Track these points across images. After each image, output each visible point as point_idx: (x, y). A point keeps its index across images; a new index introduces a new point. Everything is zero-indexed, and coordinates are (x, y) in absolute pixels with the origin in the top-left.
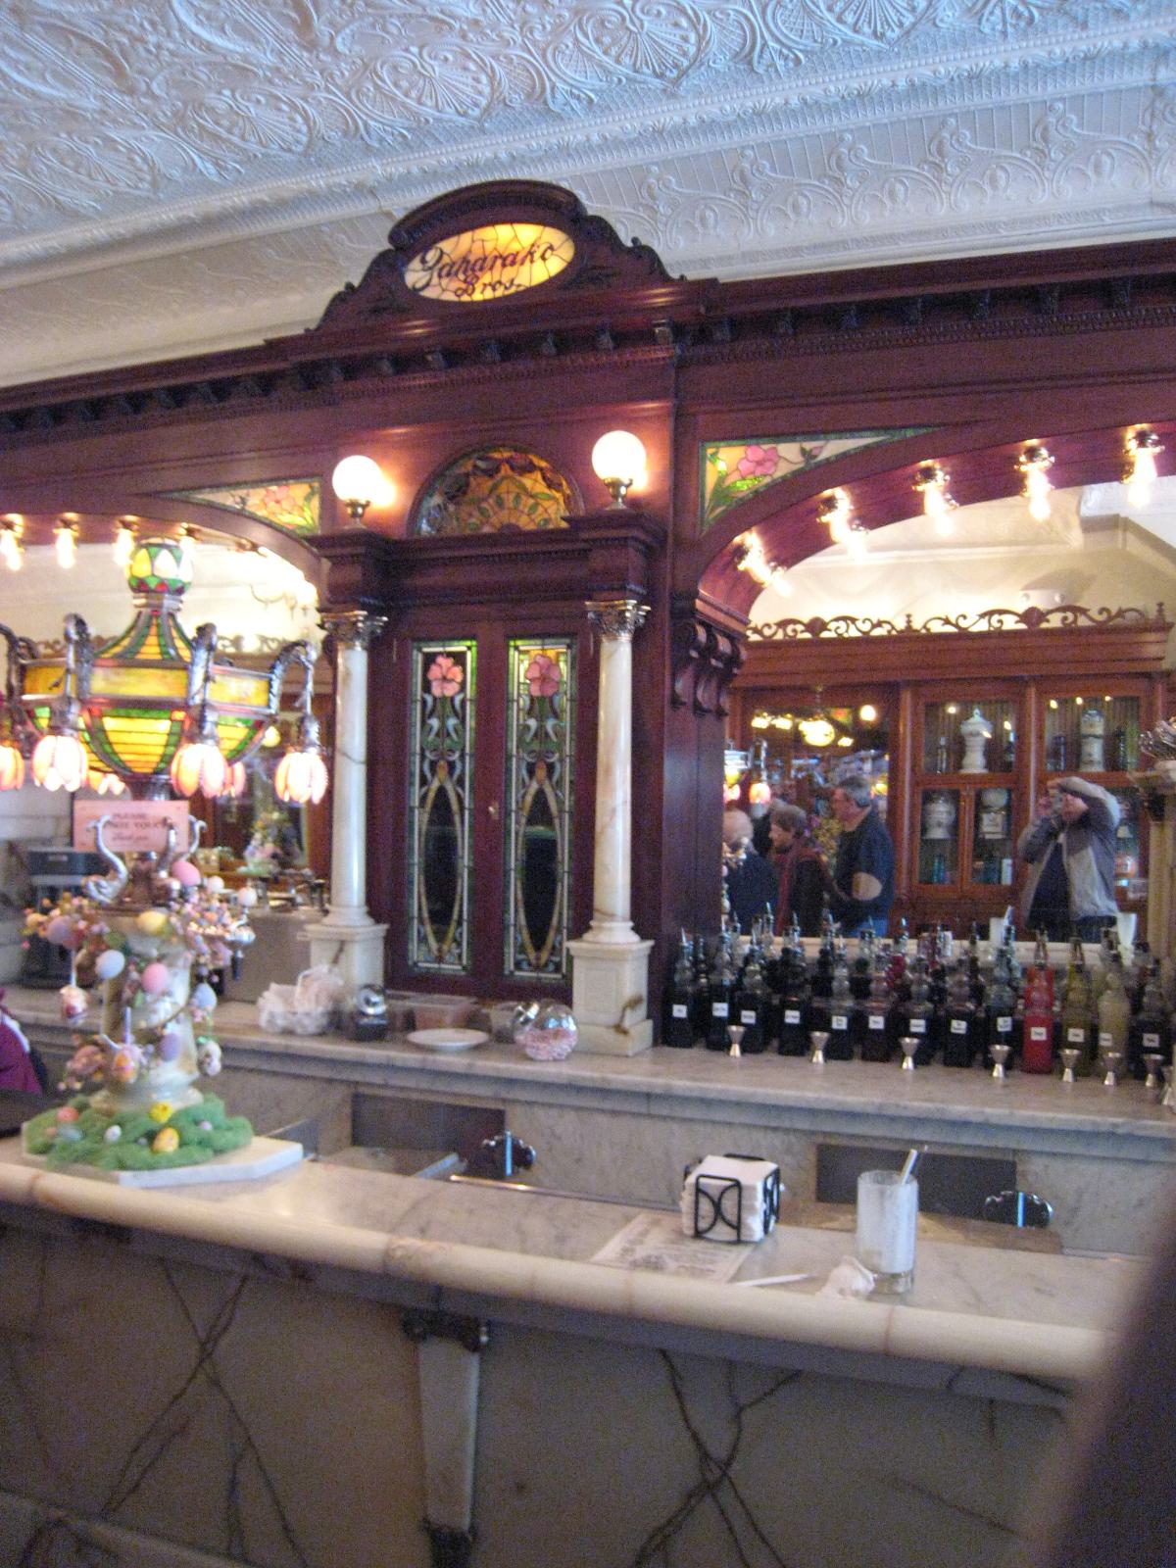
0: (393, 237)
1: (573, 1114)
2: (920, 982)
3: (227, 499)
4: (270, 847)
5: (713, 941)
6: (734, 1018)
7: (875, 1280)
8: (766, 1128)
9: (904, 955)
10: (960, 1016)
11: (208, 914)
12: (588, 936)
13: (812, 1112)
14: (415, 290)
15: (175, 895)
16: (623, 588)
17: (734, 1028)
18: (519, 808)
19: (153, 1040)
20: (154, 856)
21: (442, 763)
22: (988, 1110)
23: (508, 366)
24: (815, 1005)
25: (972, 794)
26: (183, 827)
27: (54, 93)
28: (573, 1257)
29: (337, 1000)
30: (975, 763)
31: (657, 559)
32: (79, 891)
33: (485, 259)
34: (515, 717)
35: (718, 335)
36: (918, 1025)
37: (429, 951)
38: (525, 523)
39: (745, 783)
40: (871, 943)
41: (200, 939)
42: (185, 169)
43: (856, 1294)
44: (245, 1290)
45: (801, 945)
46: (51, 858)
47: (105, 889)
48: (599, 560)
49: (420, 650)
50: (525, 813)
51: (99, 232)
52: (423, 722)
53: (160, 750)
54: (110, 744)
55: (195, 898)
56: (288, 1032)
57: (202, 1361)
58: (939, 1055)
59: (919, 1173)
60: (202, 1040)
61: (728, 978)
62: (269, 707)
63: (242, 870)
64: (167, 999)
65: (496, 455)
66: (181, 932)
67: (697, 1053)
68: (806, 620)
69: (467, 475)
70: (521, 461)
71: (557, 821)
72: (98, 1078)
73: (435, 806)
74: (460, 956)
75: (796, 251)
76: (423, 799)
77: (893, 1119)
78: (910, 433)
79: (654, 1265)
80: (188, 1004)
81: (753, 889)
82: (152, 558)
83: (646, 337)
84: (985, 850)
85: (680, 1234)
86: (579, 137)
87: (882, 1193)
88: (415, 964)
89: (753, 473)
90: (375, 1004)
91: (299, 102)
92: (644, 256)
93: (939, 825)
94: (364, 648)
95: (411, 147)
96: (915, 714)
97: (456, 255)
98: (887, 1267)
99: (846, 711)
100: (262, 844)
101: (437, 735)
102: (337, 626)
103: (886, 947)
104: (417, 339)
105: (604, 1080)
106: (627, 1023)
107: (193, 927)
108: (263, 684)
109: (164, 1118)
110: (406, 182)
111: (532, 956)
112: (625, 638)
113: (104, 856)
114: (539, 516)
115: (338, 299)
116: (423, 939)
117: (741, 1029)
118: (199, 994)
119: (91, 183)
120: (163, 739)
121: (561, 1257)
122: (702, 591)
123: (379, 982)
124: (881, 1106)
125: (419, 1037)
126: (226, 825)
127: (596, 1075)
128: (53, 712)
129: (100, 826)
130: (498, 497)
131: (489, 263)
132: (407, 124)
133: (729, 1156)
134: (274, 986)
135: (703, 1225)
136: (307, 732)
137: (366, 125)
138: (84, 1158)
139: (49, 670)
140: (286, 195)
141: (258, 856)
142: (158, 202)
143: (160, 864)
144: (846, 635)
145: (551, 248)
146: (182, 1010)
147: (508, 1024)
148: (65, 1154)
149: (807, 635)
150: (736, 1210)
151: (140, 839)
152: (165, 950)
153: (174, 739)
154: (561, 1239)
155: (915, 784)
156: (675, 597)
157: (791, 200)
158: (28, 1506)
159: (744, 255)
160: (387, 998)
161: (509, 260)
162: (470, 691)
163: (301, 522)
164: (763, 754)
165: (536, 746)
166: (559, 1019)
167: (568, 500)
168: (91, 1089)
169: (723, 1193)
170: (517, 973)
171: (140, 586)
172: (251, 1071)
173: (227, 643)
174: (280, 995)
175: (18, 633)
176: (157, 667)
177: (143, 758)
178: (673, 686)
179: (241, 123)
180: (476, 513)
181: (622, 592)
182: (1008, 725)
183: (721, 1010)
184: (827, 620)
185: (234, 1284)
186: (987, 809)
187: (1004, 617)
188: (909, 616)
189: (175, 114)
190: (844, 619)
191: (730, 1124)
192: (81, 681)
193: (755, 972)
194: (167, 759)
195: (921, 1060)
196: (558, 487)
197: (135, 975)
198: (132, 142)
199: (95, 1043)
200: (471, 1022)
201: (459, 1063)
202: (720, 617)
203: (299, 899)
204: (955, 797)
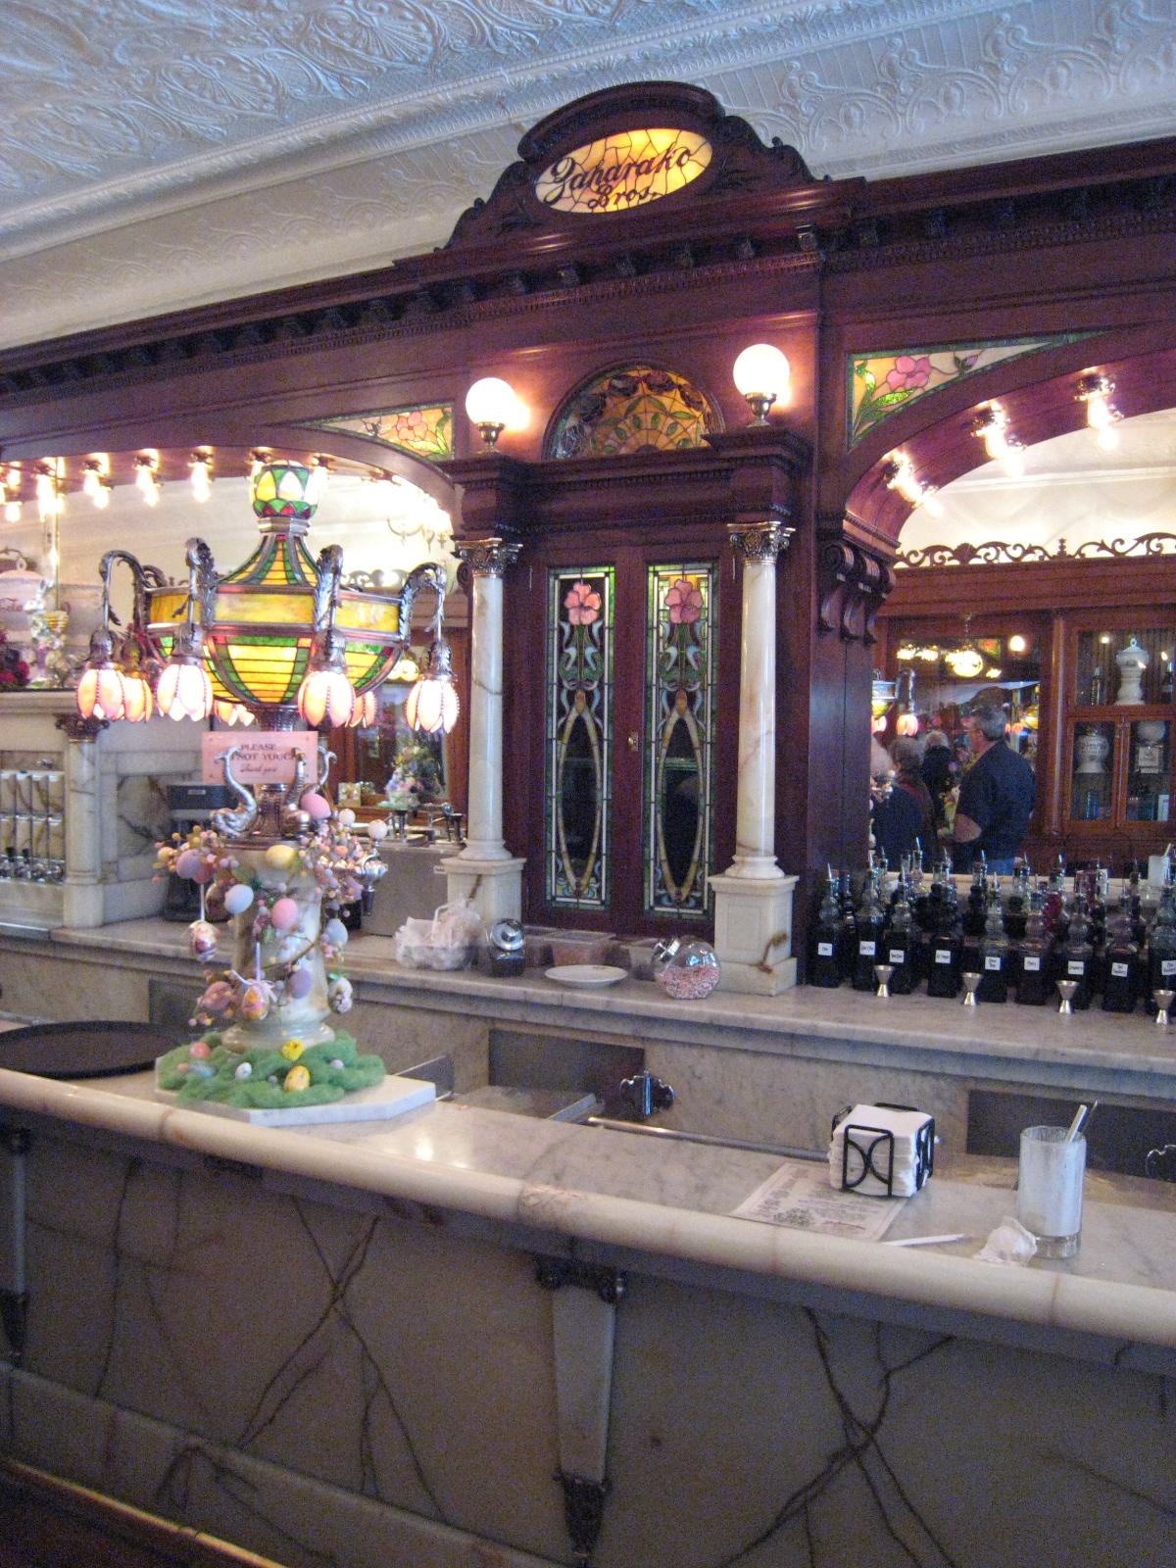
0: (522, 149)
1: (714, 1054)
2: (1079, 922)
3: (358, 426)
4: (410, 781)
5: (861, 877)
6: (882, 957)
7: (1037, 1243)
8: (915, 1072)
9: (1061, 893)
10: (1121, 959)
11: (339, 848)
12: (729, 871)
13: (963, 1057)
14: (547, 204)
15: (304, 827)
16: (767, 510)
17: (881, 968)
18: (658, 741)
19: (284, 976)
20: (283, 787)
21: (580, 693)
22: (1153, 1059)
23: (646, 280)
24: (967, 944)
25: (1128, 725)
26: (311, 758)
27: (176, 12)
28: (712, 1210)
29: (474, 935)
30: (1131, 694)
31: (804, 477)
32: (207, 825)
33: (619, 167)
34: (655, 646)
35: (865, 239)
36: (1076, 968)
37: (568, 884)
38: (663, 443)
39: (892, 716)
40: (1025, 880)
41: (330, 872)
42: (310, 88)
43: (1017, 1257)
44: (377, 1231)
45: (952, 882)
46: (190, 792)
47: (235, 822)
48: (743, 479)
49: (556, 577)
50: (666, 744)
51: (223, 159)
52: (561, 651)
53: (287, 679)
54: (236, 672)
55: (324, 830)
56: (424, 967)
57: (334, 1301)
58: (1099, 998)
59: (1087, 1130)
60: (332, 976)
61: (876, 915)
62: (399, 633)
63: (384, 804)
64: (298, 934)
65: (634, 374)
66: (311, 865)
67: (843, 992)
68: (954, 547)
69: (604, 396)
70: (659, 380)
71: (698, 752)
72: (229, 1013)
73: (573, 738)
74: (599, 891)
75: (948, 147)
76: (561, 730)
77: (1050, 1065)
78: (1072, 338)
79: (799, 1220)
80: (319, 939)
81: (905, 826)
82: (277, 482)
83: (788, 243)
84: (1141, 785)
85: (827, 1185)
86: (716, 32)
87: (1047, 1152)
88: (554, 898)
89: (903, 385)
90: (512, 939)
91: (423, 9)
92: (785, 154)
93: (1092, 759)
94: (500, 576)
95: (540, 53)
96: (1068, 644)
97: (589, 165)
98: (1051, 1231)
99: (995, 642)
100: (403, 779)
101: (575, 664)
102: (471, 553)
103: (1043, 885)
104: (553, 253)
105: (746, 1019)
106: (770, 962)
107: (323, 860)
108: (392, 610)
109: (295, 1056)
110: (535, 89)
111: (673, 890)
112: (769, 561)
113: (233, 787)
114: (678, 436)
115: (467, 216)
116: (561, 874)
117: (890, 969)
118: (330, 929)
119: (215, 106)
120: (289, 667)
121: (702, 1209)
122: (850, 512)
123: (517, 917)
124: (1037, 1052)
125: (557, 973)
126: (368, 759)
127: (739, 1014)
128: (176, 640)
129: (228, 757)
130: (635, 417)
131: (622, 171)
132: (535, 27)
133: (879, 1105)
134: (410, 921)
135: (852, 1177)
136: (438, 659)
137: (492, 29)
138: (213, 1095)
139: (175, 598)
140: (413, 110)
141: (399, 792)
142: (284, 125)
143: (289, 797)
144: (996, 562)
145: (687, 152)
146: (313, 945)
147: (648, 960)
148: (195, 1091)
149: (956, 562)
150: (887, 1165)
151: (267, 770)
152: (293, 885)
153: (301, 666)
154: (702, 1189)
155: (1066, 718)
156: (821, 516)
157: (942, 91)
158: (168, 1433)
159: (891, 153)
160: (525, 934)
161: (644, 167)
162: (608, 619)
163: (435, 448)
164: (911, 685)
165: (676, 674)
166: (700, 956)
167: (708, 418)
168: (221, 1024)
169: (874, 1145)
170: (657, 909)
171: (265, 510)
172: (389, 1005)
173: (366, 578)
174: (415, 928)
175: (142, 563)
176: (280, 593)
177: (270, 687)
178: (820, 612)
179: (364, 35)
180: (613, 435)
181: (767, 512)
182: (1164, 656)
183: (868, 948)
184: (976, 546)
185: (367, 1225)
186: (1144, 742)
187: (1164, 542)
188: (1062, 541)
189: (297, 28)
190: (995, 545)
191: (877, 1067)
192: (206, 608)
193: (903, 911)
194: (294, 688)
195: (1078, 1004)
196: (698, 406)
197: (264, 910)
198: (256, 61)
199: (226, 979)
200: (610, 958)
201: (598, 1000)
202: (868, 539)
203: (437, 833)
204: (1108, 731)
